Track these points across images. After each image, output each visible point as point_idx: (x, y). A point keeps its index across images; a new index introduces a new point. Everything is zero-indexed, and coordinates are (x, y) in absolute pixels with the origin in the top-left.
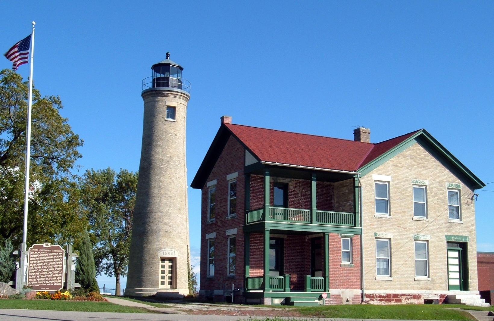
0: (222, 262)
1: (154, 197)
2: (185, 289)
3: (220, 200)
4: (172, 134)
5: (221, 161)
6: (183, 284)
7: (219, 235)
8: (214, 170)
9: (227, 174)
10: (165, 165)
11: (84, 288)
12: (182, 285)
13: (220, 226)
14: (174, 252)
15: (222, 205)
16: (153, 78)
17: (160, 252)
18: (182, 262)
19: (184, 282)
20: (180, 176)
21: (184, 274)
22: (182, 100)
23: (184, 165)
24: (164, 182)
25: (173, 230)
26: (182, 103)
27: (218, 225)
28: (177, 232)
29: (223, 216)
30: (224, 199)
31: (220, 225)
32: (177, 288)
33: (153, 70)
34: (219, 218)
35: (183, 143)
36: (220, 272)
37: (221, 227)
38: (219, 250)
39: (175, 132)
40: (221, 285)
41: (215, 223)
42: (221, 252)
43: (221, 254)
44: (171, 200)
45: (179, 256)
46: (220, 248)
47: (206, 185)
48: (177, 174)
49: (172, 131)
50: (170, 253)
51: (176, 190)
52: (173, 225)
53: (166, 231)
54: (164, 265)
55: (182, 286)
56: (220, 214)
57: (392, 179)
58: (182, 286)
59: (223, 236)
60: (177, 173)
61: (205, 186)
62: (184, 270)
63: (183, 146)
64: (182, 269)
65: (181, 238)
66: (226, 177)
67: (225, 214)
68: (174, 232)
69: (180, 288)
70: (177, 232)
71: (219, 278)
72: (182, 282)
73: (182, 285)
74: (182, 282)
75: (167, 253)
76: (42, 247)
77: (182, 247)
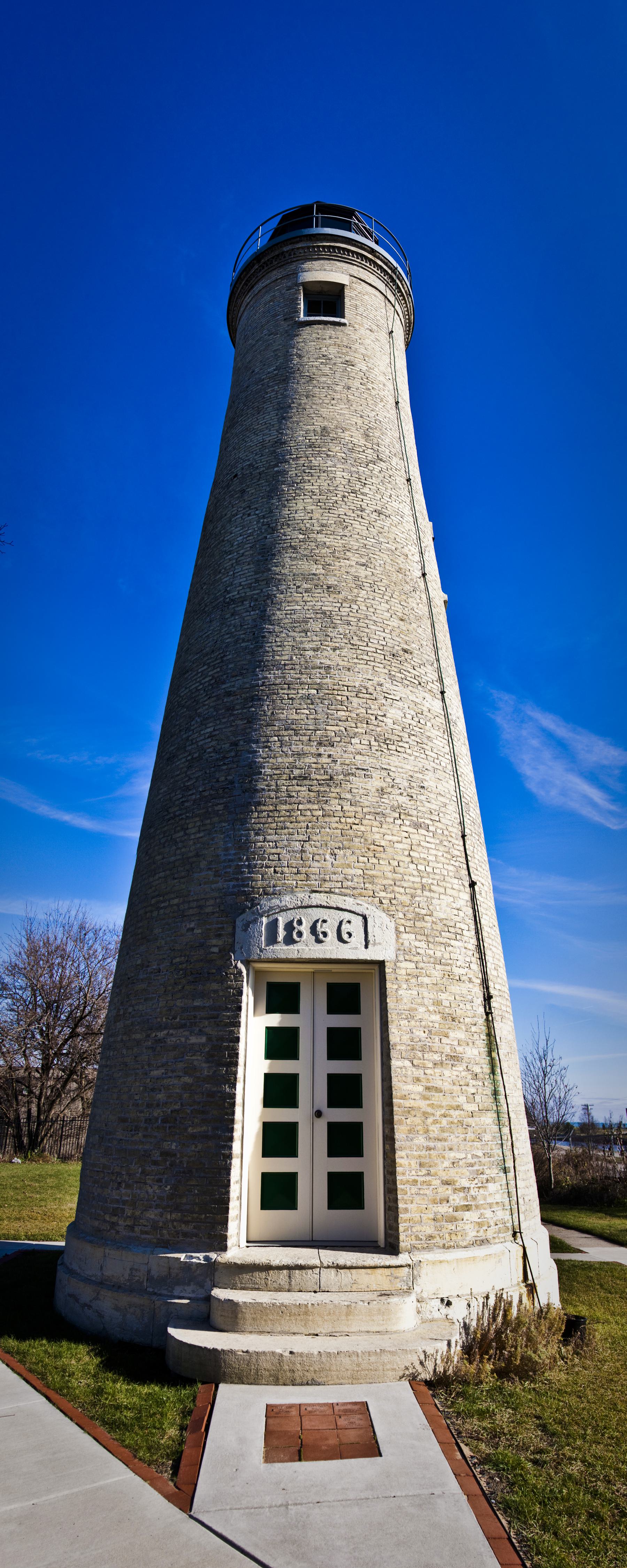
1: (289, 726)
2: (484, 1242)
6: (457, 1199)
11: (618, 1198)
12: (443, 1209)
14: (358, 921)
19: (465, 1183)
21: (462, 1099)
23: (409, 480)
24: (288, 525)
32: (402, 1245)
44: (328, 603)
50: (326, 928)
53: (297, 772)
54: (334, 1151)
55: (452, 1220)
57: (558, 1262)
58: (452, 1220)
64: (436, 1057)
68: (357, 782)
69: (428, 1243)
72: (447, 1183)
73: (443, 1209)
74: (447, 1183)
75: (305, 928)
76: (562, 1324)
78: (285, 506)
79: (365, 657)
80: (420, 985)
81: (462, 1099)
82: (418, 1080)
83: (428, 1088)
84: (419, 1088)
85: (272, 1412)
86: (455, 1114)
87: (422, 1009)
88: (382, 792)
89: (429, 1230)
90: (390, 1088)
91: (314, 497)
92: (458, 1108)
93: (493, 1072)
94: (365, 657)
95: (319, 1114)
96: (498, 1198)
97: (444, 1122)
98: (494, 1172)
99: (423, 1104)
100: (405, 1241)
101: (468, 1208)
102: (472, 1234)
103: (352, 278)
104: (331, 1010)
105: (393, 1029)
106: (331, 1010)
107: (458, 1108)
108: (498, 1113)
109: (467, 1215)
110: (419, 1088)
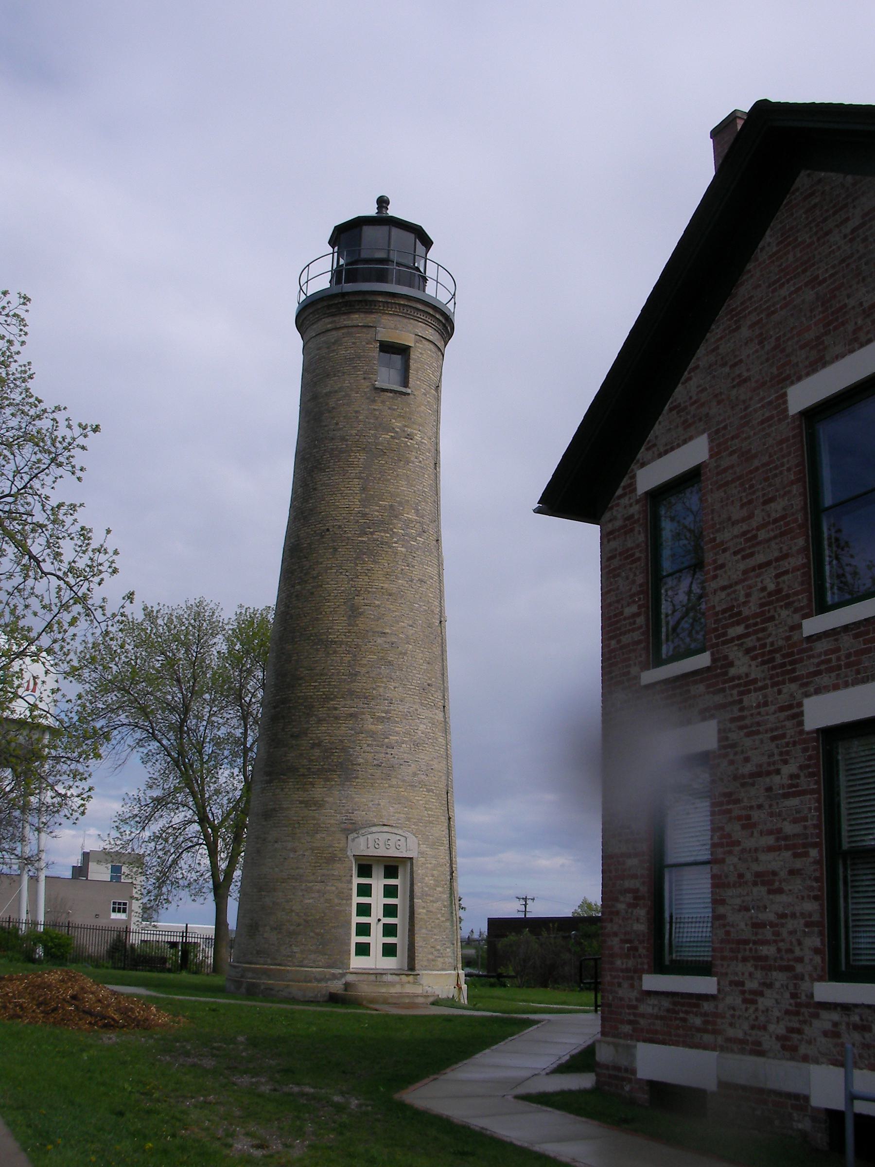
0: (780, 891)
3: (744, 534)
4: (396, 432)
5: (738, 328)
7: (748, 735)
8: (680, 393)
9: (788, 377)
10: (372, 533)
12: (430, 957)
13: (755, 681)
15: (760, 558)
16: (335, 266)
17: (353, 840)
18: (433, 876)
19: (439, 947)
20: (424, 575)
21: (439, 916)
22: (431, 331)
25: (401, 762)
26: (431, 338)
27: (733, 679)
28: (413, 767)
29: (772, 618)
30: (776, 521)
31: (753, 676)
32: (416, 968)
33: (336, 249)
34: (739, 637)
35: (432, 465)
36: (765, 950)
37: (760, 684)
38: (749, 817)
39: (406, 426)
40: (780, 1029)
41: (708, 669)
42: (770, 833)
43: (770, 840)
45: (421, 853)
46: (760, 807)
47: (632, 487)
48: (413, 567)
49: (397, 424)
51: (411, 623)
52: (400, 743)
53: (376, 762)
56: (746, 612)
59: (773, 739)
60: (415, 563)
61: (619, 492)
62: (439, 904)
63: (433, 477)
65: (429, 791)
66: (785, 395)
67: (787, 606)
69: (426, 968)
70: (413, 767)
71: (752, 985)
72: (432, 947)
73: (430, 957)
74: (432, 947)
77: (431, 822)
78: (180, 777)
79: (410, 693)
80: (427, 868)
81: (439, 916)
82: (424, 908)
83: (427, 911)
84: (425, 911)
85: (357, 954)
86: (437, 921)
87: (426, 878)
88: (415, 774)
89: (425, 963)
90: (413, 913)
91: (385, 570)
92: (438, 919)
93: (451, 903)
94: (410, 693)
95: (379, 920)
96: (450, 954)
97: (433, 924)
98: (448, 944)
99: (425, 917)
100: (417, 966)
101: (439, 957)
102: (440, 966)
103: (417, 337)
104: (385, 896)
105: (415, 887)
106: (385, 896)
107: (438, 919)
108: (452, 921)
109: (439, 959)
110: (425, 911)
